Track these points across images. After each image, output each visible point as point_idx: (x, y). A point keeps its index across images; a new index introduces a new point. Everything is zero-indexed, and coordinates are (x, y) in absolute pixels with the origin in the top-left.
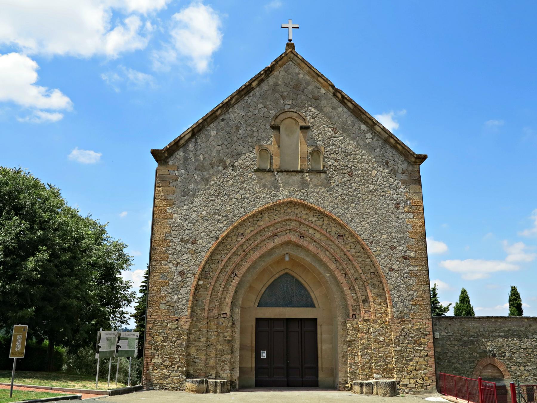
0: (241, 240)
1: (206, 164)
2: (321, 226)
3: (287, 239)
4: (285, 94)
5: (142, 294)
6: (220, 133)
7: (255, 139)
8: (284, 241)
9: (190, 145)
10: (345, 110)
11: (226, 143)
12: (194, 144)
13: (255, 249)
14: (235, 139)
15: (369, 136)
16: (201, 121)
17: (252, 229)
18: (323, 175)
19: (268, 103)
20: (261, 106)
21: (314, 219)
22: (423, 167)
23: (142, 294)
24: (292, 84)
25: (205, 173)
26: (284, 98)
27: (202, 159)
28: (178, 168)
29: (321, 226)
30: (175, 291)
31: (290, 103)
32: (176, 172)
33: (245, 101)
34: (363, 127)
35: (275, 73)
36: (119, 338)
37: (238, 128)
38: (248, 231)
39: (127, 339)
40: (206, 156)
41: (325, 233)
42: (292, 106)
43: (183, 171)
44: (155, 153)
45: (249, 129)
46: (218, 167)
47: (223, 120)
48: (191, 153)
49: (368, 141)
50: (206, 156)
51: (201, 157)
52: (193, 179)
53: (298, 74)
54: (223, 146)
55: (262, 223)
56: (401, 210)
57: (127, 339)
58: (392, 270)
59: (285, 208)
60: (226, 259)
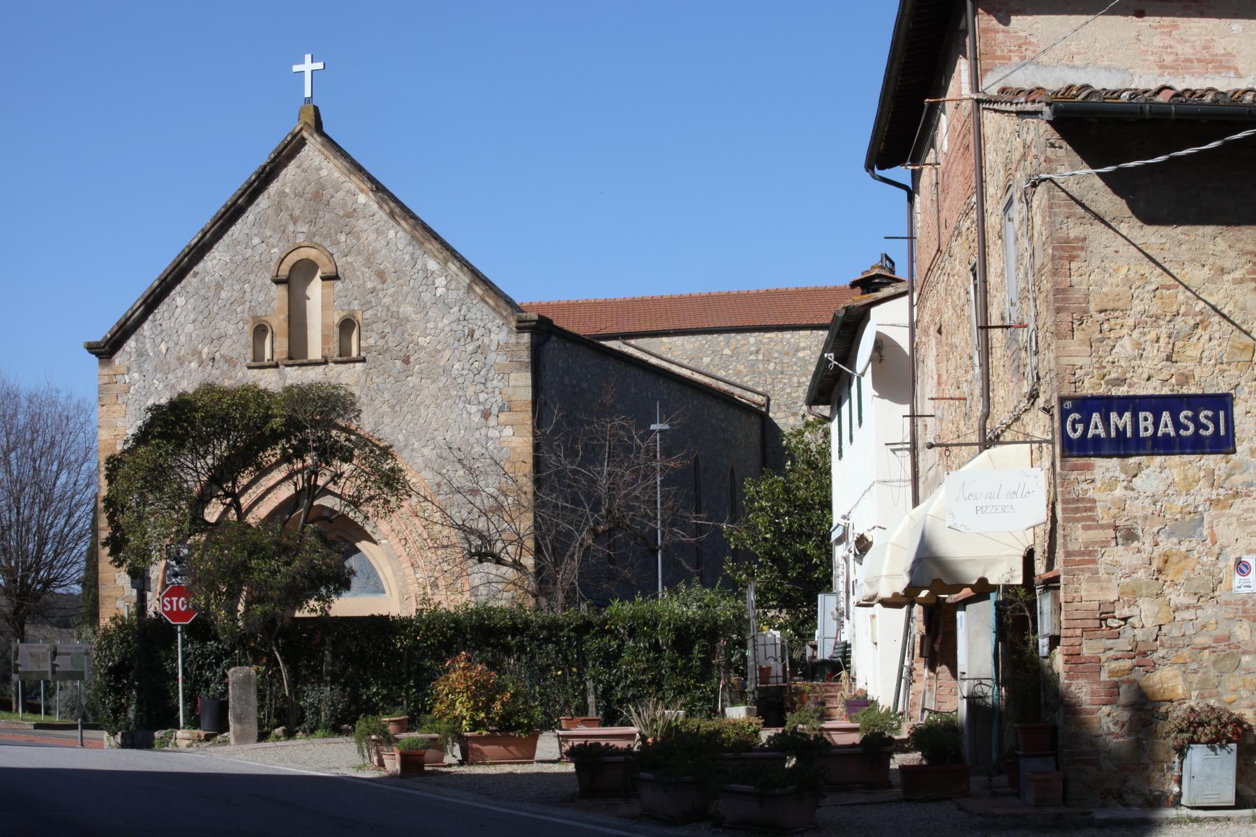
1: (171, 358)
4: (297, 212)
5: (358, 545)
6: (192, 301)
7: (248, 304)
14: (216, 308)
16: (156, 283)
18: (359, 366)
20: (256, 241)
23: (358, 545)
24: (311, 189)
26: (295, 220)
28: (129, 369)
31: (305, 229)
36: (55, 654)
37: (219, 287)
39: (68, 654)
40: (171, 344)
42: (310, 236)
43: (136, 376)
44: (92, 348)
45: (237, 287)
48: (147, 341)
49: (440, 291)
50: (171, 344)
52: (153, 389)
57: (68, 654)
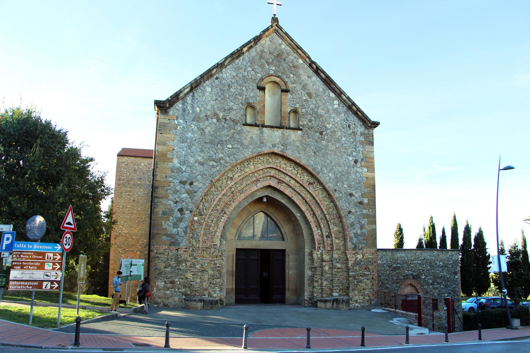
3: (268, 184)
10: (318, 79)
11: (219, 99)
13: (241, 192)
15: (336, 102)
21: (291, 169)
25: (201, 124)
27: (198, 111)
30: (175, 225)
31: (274, 69)
32: (176, 121)
33: (236, 63)
34: (332, 95)
35: (262, 42)
46: (212, 119)
47: (217, 78)
49: (336, 106)
51: (198, 110)
53: (280, 45)
58: (350, 212)
60: (218, 199)
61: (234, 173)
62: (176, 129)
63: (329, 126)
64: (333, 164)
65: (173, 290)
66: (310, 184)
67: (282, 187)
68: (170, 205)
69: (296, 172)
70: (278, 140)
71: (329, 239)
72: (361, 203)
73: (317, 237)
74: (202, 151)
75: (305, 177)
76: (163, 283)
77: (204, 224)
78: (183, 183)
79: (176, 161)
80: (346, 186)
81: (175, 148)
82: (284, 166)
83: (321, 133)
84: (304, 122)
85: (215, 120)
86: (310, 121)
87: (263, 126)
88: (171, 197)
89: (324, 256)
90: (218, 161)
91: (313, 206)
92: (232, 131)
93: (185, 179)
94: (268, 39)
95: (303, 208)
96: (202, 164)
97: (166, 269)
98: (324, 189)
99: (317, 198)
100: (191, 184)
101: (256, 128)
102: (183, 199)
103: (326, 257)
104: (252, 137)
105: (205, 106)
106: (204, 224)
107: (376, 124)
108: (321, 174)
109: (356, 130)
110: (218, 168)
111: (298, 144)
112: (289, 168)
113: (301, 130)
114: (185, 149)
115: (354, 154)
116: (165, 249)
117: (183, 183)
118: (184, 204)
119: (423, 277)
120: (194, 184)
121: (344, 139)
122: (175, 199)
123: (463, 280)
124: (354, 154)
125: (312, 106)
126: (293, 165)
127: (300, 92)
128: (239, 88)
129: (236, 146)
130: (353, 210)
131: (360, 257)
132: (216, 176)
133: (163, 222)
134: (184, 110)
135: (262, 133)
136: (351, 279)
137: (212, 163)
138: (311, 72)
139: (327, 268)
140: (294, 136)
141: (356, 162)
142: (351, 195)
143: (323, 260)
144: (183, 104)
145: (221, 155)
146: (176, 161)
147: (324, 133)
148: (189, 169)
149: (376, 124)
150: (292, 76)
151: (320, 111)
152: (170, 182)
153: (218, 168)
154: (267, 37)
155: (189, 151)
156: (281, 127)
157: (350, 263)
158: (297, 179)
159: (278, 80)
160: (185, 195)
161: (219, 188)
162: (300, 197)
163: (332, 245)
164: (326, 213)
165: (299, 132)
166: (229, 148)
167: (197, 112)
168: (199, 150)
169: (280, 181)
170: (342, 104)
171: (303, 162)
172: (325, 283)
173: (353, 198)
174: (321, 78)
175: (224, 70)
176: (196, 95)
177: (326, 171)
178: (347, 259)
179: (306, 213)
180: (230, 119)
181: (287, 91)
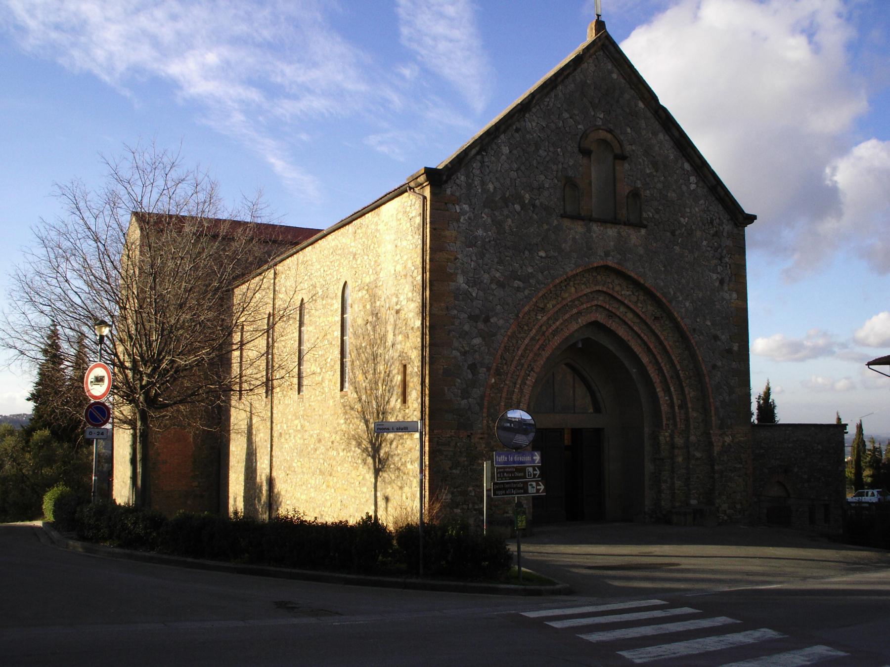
0: (542, 318)
2: (636, 303)
3: (593, 319)
8: (589, 321)
9: (474, 165)
10: (667, 137)
11: (523, 168)
12: (479, 164)
13: (555, 333)
15: (693, 179)
17: (554, 302)
19: (576, 112)
21: (628, 293)
22: (749, 229)
25: (497, 213)
27: (491, 190)
29: (636, 303)
30: (465, 394)
31: (602, 116)
32: (457, 207)
33: (546, 103)
34: (687, 166)
35: (584, 66)
38: (550, 306)
41: (640, 313)
46: (513, 204)
47: (517, 130)
49: (693, 187)
51: (491, 187)
53: (611, 72)
54: (520, 172)
55: (567, 295)
56: (726, 288)
58: (714, 367)
59: (595, 274)
60: (523, 347)
61: (546, 301)
62: (458, 221)
63: (683, 221)
64: (691, 285)
65: (465, 507)
66: (656, 318)
67: (613, 325)
68: (455, 357)
69: (634, 298)
70: (612, 243)
71: (682, 411)
72: (729, 351)
73: (664, 408)
74: (500, 262)
75: (649, 307)
76: (449, 496)
77: (505, 390)
78: (473, 318)
79: (461, 279)
80: (709, 323)
81: (459, 256)
82: (617, 288)
83: (673, 233)
84: (648, 214)
85: (517, 207)
86: (657, 211)
87: (591, 220)
88: (456, 344)
89: (677, 440)
90: (525, 279)
91: (658, 357)
92: (545, 227)
93: (477, 312)
94: (591, 61)
95: (645, 360)
96: (501, 285)
97: (454, 471)
98: (677, 327)
99: (666, 343)
100: (487, 320)
101: (581, 223)
102: (476, 348)
103: (679, 441)
104: (574, 239)
105: (502, 181)
106: (505, 390)
107: (751, 218)
108: (674, 303)
109: (721, 228)
110: (527, 292)
111: (641, 251)
112: (624, 293)
113: (645, 227)
114: (474, 258)
115: (719, 269)
116: (451, 437)
117: (473, 318)
118: (477, 356)
119: (796, 470)
120: (492, 320)
121: (705, 243)
122: (463, 347)
123: (811, 480)
124: (719, 269)
125: (660, 186)
126: (632, 286)
127: (641, 160)
128: (552, 149)
129: (552, 253)
130: (719, 364)
131: (728, 439)
132: (523, 306)
133: (446, 388)
134: (469, 186)
135: (589, 230)
136: (717, 476)
137: (517, 283)
138: (657, 126)
139: (680, 459)
140: (635, 237)
141: (722, 282)
142: (716, 338)
143: (673, 446)
144: (467, 177)
145: (530, 270)
146: (461, 279)
147: (677, 233)
148: (481, 293)
149: (751, 218)
150: (629, 130)
151: (672, 195)
152: (454, 317)
153: (527, 292)
154: (590, 57)
155: (481, 261)
156: (614, 221)
157: (716, 450)
158: (638, 311)
159: (609, 136)
160: (477, 341)
161: (526, 328)
162: (639, 341)
163: (687, 420)
164: (678, 367)
165: (643, 231)
166: (541, 257)
167: (489, 190)
168: (496, 260)
169: (611, 315)
170: (701, 184)
171: (649, 283)
172: (678, 483)
173: (719, 343)
174: (672, 137)
175: (527, 115)
176: (486, 160)
177: (680, 299)
178: (711, 444)
179: (648, 368)
180: (541, 203)
181: (622, 157)
